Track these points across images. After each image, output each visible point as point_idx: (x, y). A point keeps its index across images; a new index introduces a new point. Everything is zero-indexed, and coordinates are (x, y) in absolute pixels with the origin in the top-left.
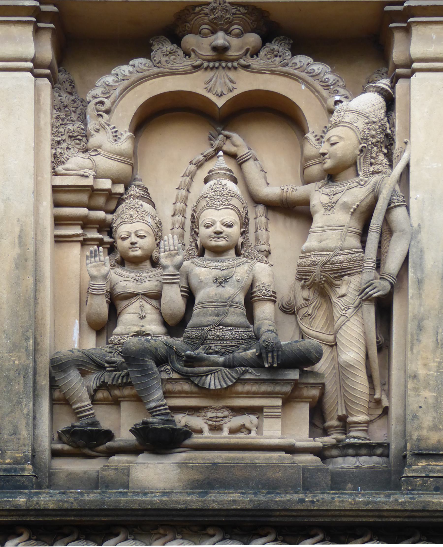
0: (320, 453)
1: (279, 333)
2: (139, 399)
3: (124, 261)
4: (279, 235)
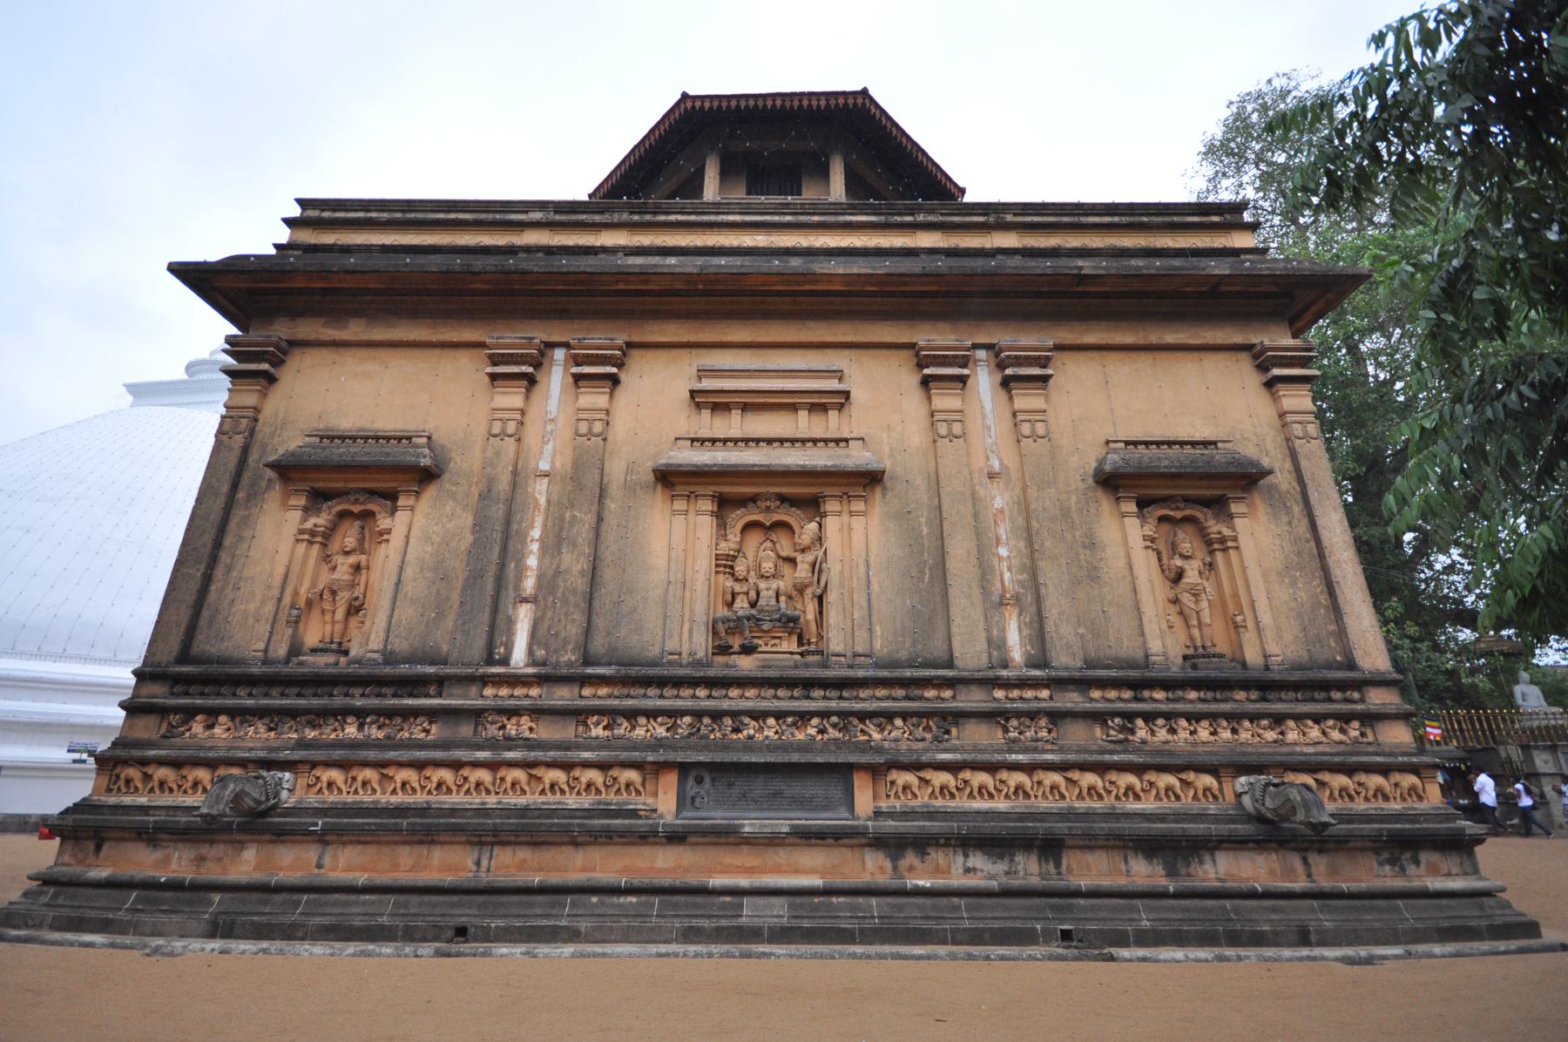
0: (801, 654)
1: (612, 412)
2: (741, 633)
3: (737, 580)
4: (786, 569)
